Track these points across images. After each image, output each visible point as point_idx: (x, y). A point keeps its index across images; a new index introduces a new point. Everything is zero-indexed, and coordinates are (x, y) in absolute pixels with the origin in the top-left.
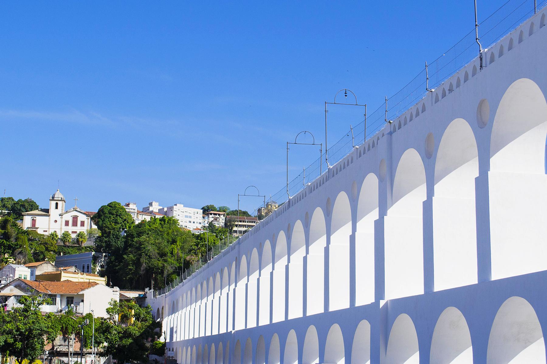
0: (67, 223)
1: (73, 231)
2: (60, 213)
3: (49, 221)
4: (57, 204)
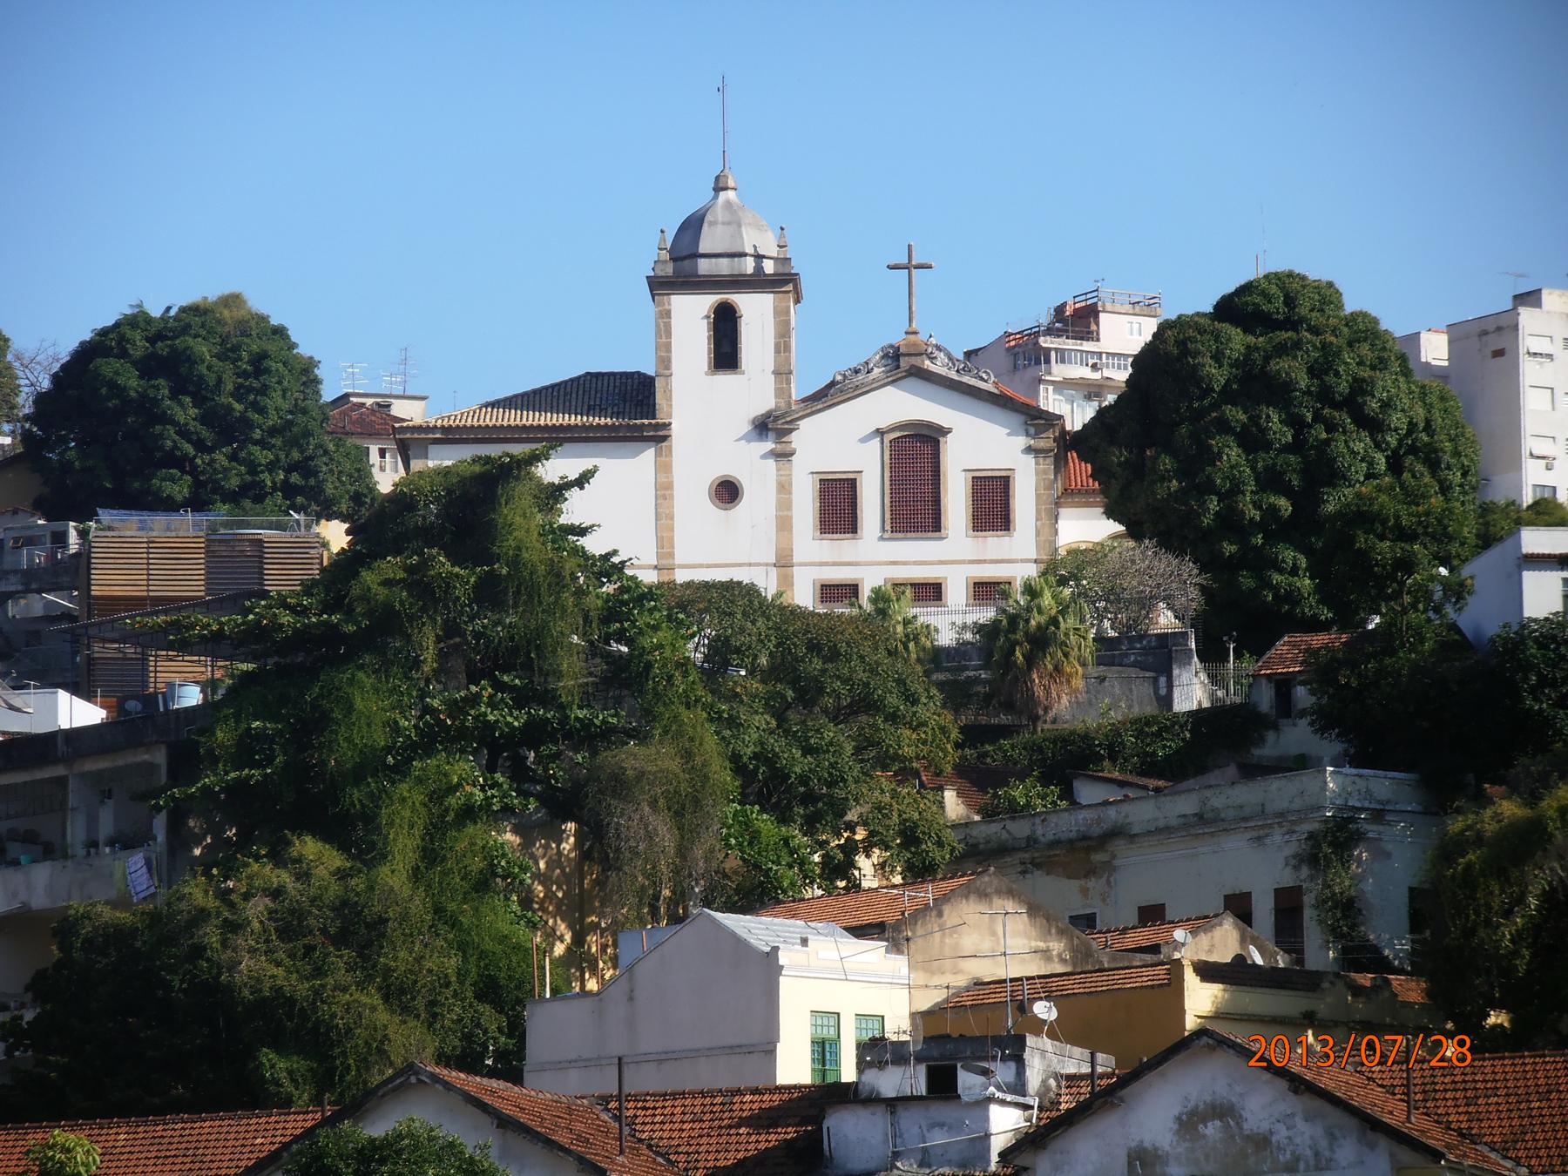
0: (838, 506)
1: (956, 574)
2: (765, 401)
3: (664, 491)
4: (725, 326)
